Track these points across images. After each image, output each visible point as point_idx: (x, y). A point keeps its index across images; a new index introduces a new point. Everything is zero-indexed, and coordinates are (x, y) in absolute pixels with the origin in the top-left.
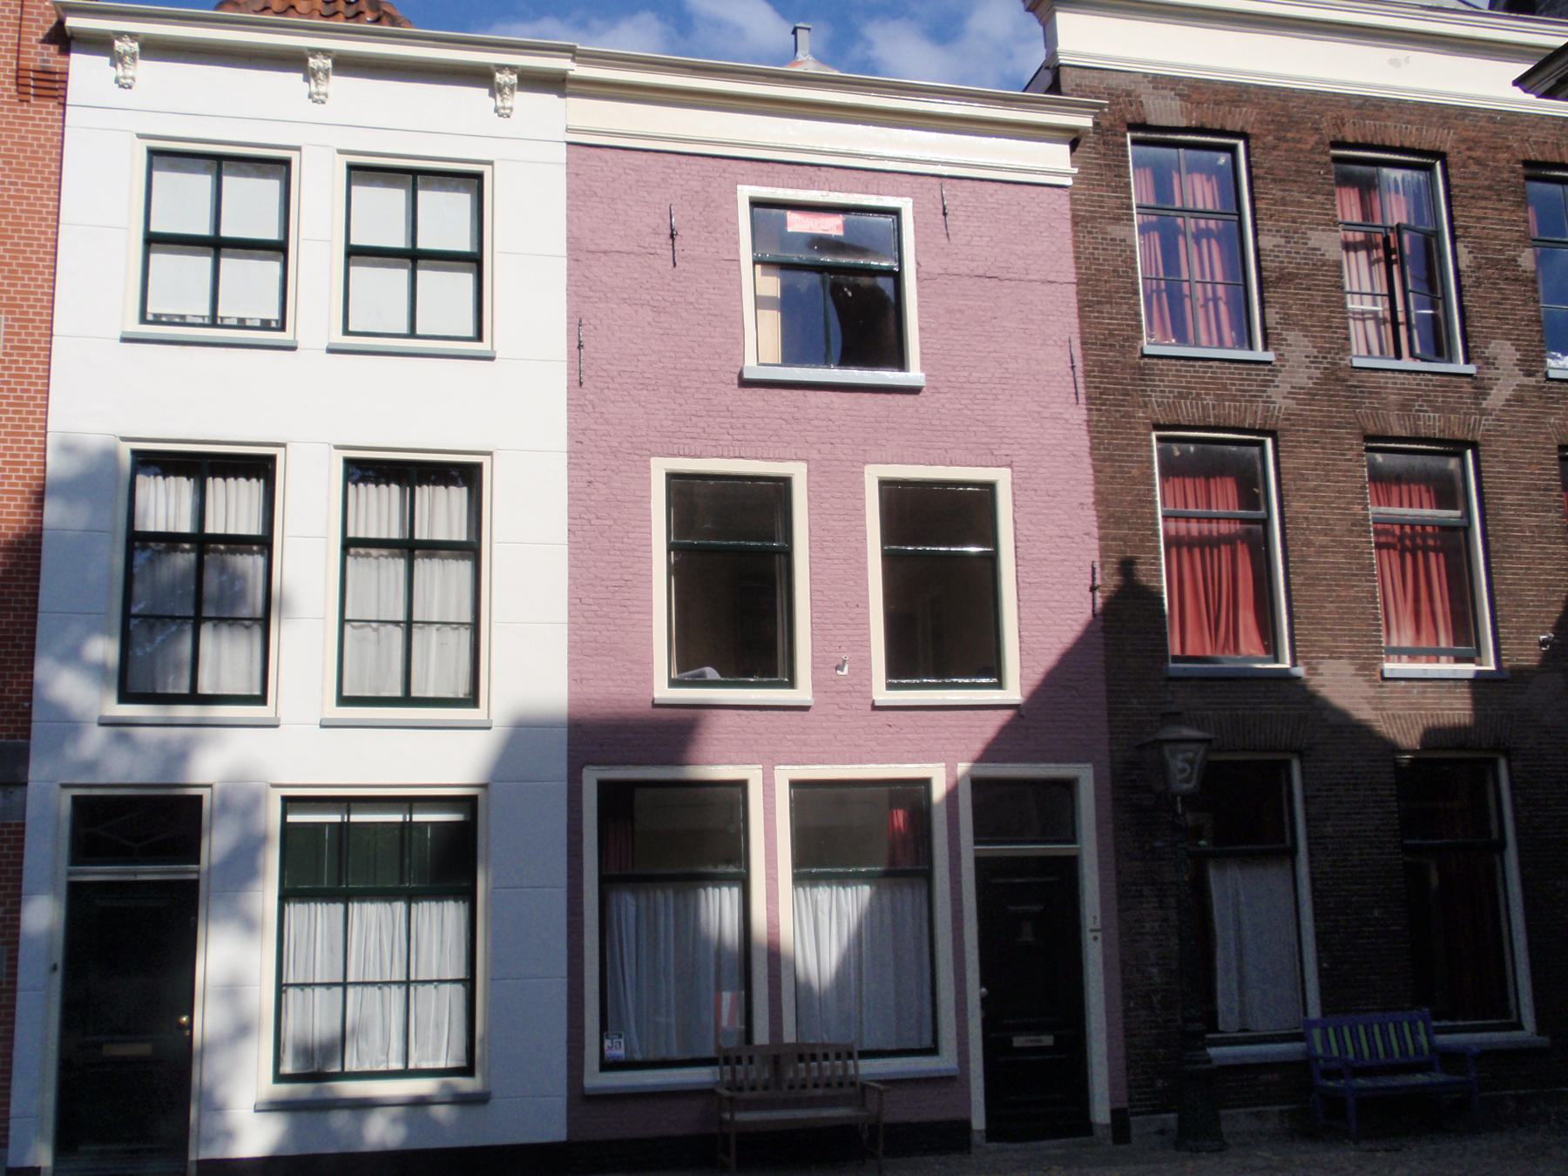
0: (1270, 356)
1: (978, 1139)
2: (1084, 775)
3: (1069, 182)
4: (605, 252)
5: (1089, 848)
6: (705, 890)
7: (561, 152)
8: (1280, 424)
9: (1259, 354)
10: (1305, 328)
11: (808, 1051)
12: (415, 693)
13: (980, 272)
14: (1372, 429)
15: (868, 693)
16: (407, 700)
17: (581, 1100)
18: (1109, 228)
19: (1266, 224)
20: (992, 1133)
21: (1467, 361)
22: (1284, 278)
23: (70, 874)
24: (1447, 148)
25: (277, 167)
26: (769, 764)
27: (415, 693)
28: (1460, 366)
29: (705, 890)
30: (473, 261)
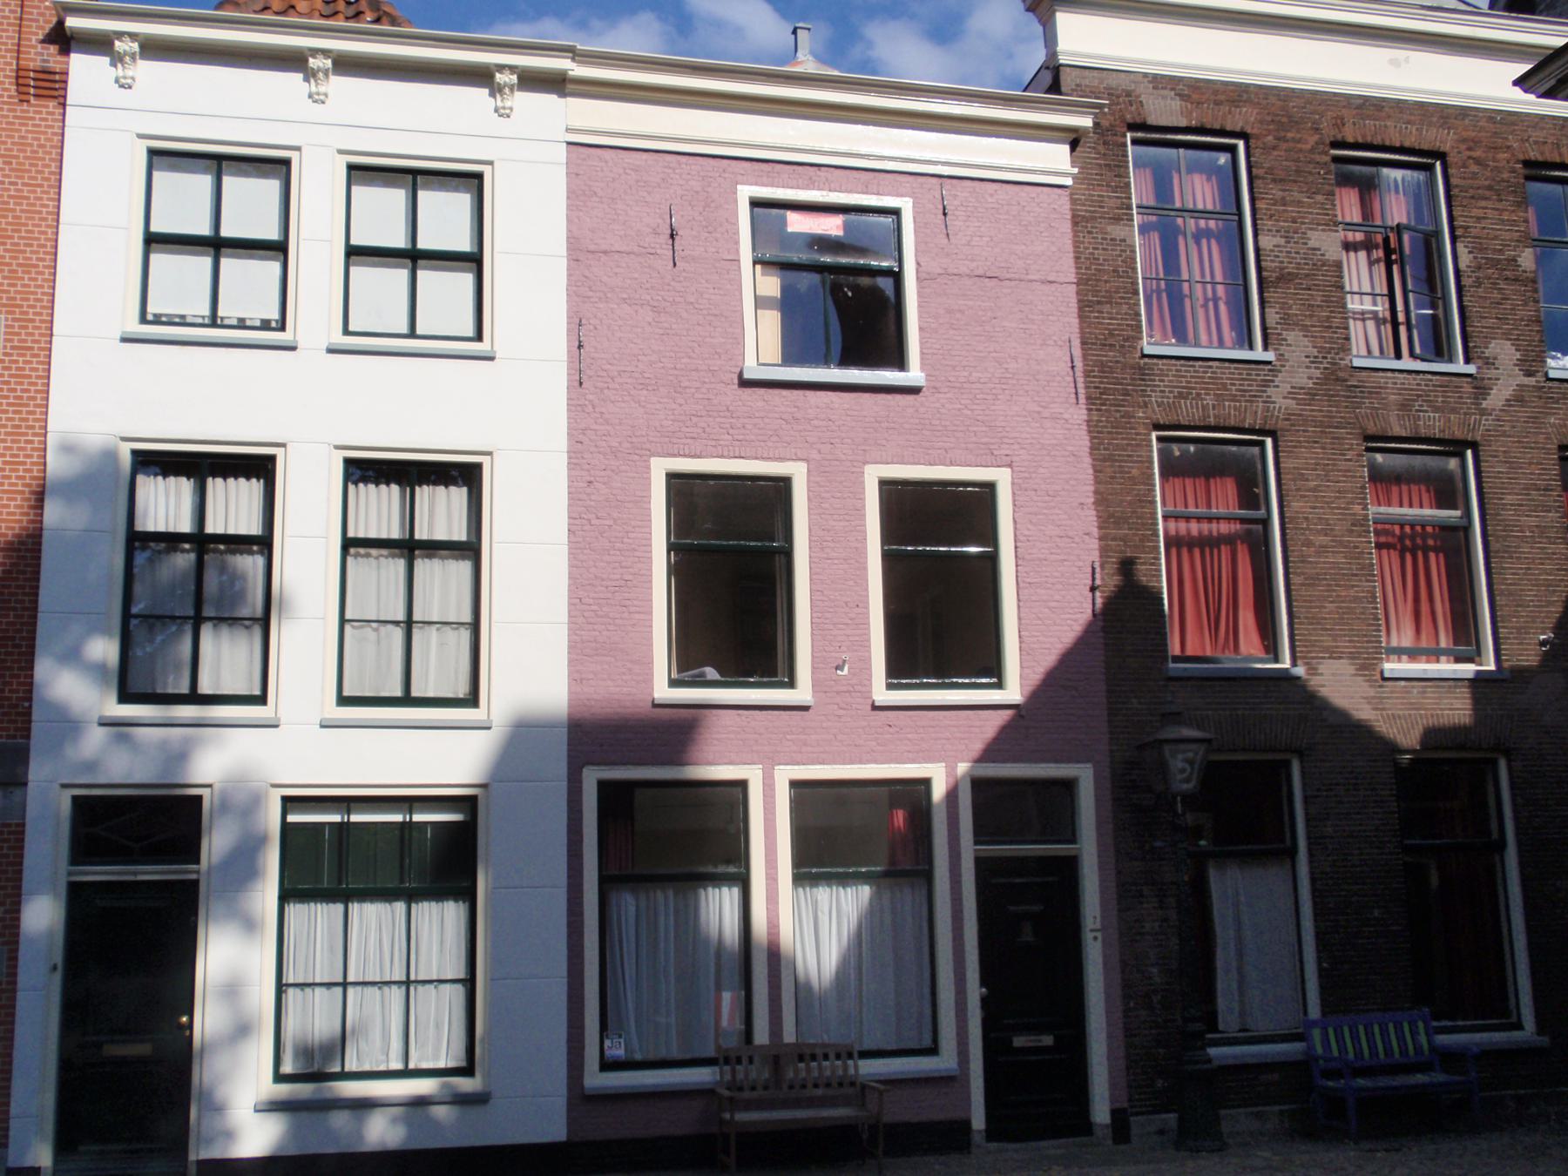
0: (1270, 356)
1: (978, 1139)
2: (1084, 775)
3: (1069, 182)
4: (605, 252)
5: (1089, 848)
6: (705, 890)
7: (561, 152)
8: (1280, 424)
9: (1259, 354)
10: (1305, 328)
11: (808, 1051)
12: (415, 693)
13: (980, 272)
14: (1372, 429)
15: (868, 693)
16: (407, 700)
17: (581, 1100)
18: (1109, 228)
19: (1266, 224)
20: (992, 1133)
21: (1467, 361)
22: (1284, 278)
23: (70, 874)
24: (1447, 148)
25: (277, 167)
26: (769, 764)
27: (415, 693)
28: (1460, 366)
29: (705, 890)
30: (473, 261)
